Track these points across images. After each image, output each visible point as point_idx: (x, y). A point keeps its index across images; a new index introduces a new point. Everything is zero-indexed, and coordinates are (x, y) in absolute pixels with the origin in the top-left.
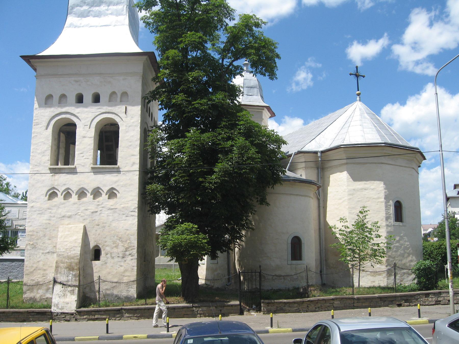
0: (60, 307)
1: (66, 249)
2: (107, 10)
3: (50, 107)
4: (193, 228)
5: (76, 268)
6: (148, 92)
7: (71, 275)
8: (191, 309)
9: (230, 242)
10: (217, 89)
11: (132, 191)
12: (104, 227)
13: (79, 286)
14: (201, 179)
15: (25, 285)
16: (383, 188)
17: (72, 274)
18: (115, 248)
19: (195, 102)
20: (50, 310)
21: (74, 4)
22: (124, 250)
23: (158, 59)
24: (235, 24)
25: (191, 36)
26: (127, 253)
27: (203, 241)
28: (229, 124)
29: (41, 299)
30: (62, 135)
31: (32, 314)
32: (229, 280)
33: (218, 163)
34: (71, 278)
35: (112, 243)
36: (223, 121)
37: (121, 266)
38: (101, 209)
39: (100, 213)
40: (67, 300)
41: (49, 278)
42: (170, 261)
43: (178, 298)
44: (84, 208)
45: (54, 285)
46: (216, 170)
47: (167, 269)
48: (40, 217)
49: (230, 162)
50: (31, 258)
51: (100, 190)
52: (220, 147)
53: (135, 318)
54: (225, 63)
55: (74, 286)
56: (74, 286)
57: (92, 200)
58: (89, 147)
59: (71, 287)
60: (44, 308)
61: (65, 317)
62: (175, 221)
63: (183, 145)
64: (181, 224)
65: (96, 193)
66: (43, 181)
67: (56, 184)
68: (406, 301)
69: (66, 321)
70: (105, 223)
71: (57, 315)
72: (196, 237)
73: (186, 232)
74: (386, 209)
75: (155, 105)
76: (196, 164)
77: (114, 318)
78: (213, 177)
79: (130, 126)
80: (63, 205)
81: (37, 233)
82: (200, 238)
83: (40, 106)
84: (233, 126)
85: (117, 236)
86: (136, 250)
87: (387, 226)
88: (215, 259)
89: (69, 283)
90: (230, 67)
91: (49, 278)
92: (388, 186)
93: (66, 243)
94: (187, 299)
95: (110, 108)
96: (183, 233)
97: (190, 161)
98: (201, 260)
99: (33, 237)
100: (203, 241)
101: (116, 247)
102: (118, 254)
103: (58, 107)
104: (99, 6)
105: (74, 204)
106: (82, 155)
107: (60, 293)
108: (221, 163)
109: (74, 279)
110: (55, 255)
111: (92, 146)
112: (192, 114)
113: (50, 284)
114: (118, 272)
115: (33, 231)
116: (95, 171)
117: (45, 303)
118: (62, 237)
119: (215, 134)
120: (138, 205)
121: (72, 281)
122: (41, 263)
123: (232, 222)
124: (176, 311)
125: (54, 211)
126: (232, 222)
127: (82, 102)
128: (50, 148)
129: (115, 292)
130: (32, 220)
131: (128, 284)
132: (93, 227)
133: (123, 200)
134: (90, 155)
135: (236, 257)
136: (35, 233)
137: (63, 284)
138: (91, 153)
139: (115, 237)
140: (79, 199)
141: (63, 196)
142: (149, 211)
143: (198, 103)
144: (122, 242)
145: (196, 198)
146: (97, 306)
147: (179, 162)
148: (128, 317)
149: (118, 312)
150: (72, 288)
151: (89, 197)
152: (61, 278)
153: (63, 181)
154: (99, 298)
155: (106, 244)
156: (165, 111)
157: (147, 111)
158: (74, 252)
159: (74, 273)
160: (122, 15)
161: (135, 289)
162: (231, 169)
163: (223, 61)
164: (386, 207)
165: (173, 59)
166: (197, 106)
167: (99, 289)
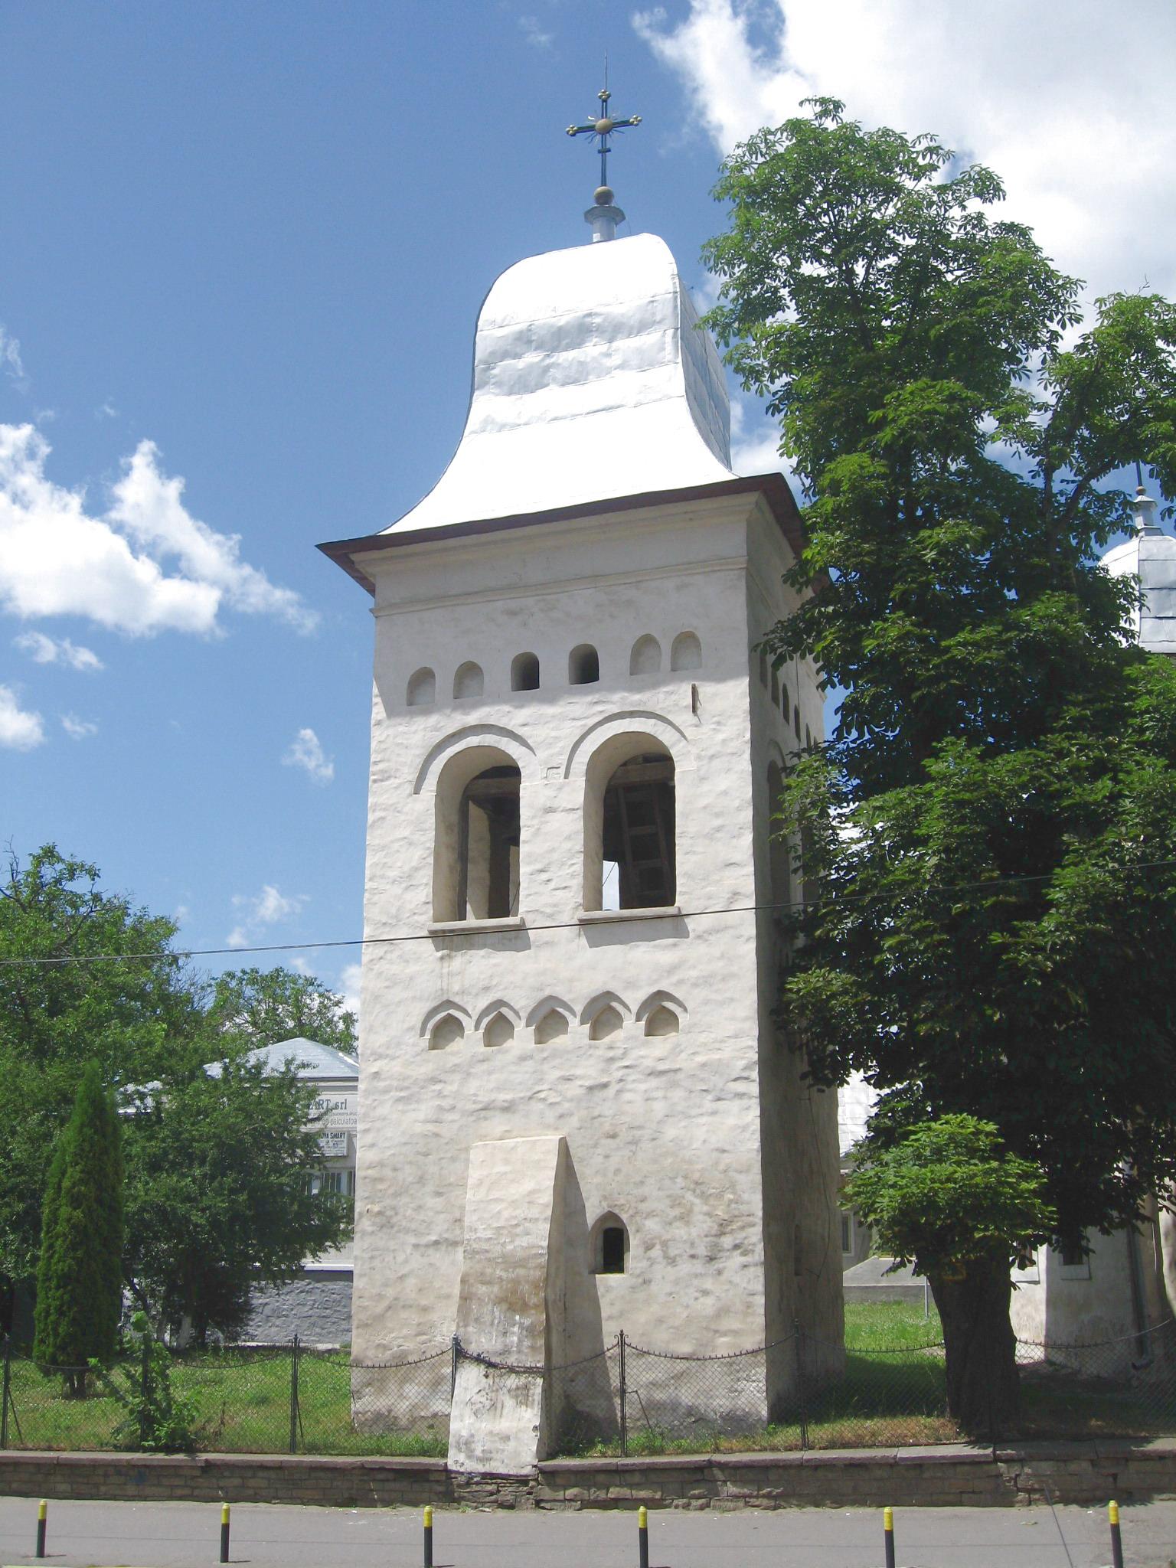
0: (478, 1453)
2: (608, 355)
3: (427, 712)
4: (977, 1133)
5: (534, 1300)
6: (770, 627)
7: (516, 1329)
8: (986, 1467)
9: (1137, 1186)
10: (1031, 588)
11: (732, 1000)
12: (635, 1142)
13: (547, 1373)
14: (996, 938)
15: (358, 1364)
17: (521, 1326)
18: (678, 1224)
19: (952, 642)
20: (442, 1461)
21: (492, 353)
22: (715, 1229)
23: (803, 503)
24: (1085, 337)
25: (914, 399)
26: (727, 1241)
27: (1024, 1185)
28: (1095, 714)
29: (413, 1421)
30: (474, 810)
31: (380, 1476)
32: (1141, 1344)
33: (1063, 868)
34: (515, 1339)
35: (668, 1202)
36: (1068, 703)
37: (706, 1293)
38: (619, 1074)
39: (619, 1092)
40: (504, 1425)
41: (439, 1338)
42: (894, 1268)
43: (933, 1421)
44: (557, 1074)
45: (455, 1369)
46: (1057, 895)
47: (889, 1307)
48: (404, 1112)
49: (1114, 859)
50: (376, 1263)
51: (614, 1004)
52: (1066, 803)
53: (765, 1502)
54: (1056, 487)
55: (530, 1371)
56: (530, 1371)
57: (587, 1041)
58: (568, 845)
59: (517, 1373)
60: (424, 1453)
61: (496, 1490)
62: (906, 1111)
63: (919, 810)
64: (929, 1120)
66: (411, 979)
67: (456, 988)
69: (502, 1506)
70: (640, 1128)
71: (468, 1484)
72: (994, 1170)
73: (955, 1149)
75: (802, 673)
76: (975, 877)
77: (681, 1502)
78: (1048, 923)
79: (712, 757)
80: (485, 1066)
81: (395, 1170)
82: (1008, 1175)
83: (391, 712)
84: (1112, 719)
85: (685, 1177)
86: (759, 1229)
88: (1080, 1262)
89: (512, 1360)
90: (1082, 504)
91: (439, 1338)
93: (498, 1207)
94: (973, 1428)
95: (637, 697)
96: (939, 1155)
97: (947, 869)
98: (1022, 1267)
99: (380, 1187)
100: (1024, 1185)
101: (681, 1218)
102: (692, 1244)
103: (455, 709)
104: (579, 345)
105: (523, 1058)
106: (544, 876)
107: (477, 1398)
108: (1076, 865)
109: (527, 1343)
110: (461, 1249)
111: (579, 843)
112: (943, 686)
113: (441, 1365)
114: (695, 1315)
115: (381, 1164)
116: (595, 928)
117: (428, 1437)
118: (480, 1183)
119: (1042, 754)
120: (759, 1053)
121: (519, 1352)
122: (411, 1282)
123: (1138, 1108)
124: (926, 1475)
125: (449, 1089)
126: (1138, 1108)
128: (431, 860)
129: (686, 1396)
130: (378, 1124)
131: (731, 1361)
132: (595, 1146)
133: (702, 1038)
134: (573, 876)
135: (1164, 1251)
136: (388, 1172)
137: (490, 1365)
138: (572, 871)
139: (679, 1180)
140: (539, 1042)
141: (481, 1031)
142: (804, 1076)
143: (965, 644)
144: (704, 1197)
145: (982, 1015)
146: (619, 1451)
147: (907, 877)
148: (736, 1497)
149: (699, 1476)
150: (522, 1380)
151: (577, 1030)
152: (482, 1342)
153: (484, 974)
154: (623, 1418)
155: (644, 1207)
156: (839, 695)
157: (775, 699)
158: (524, 1241)
159: (527, 1322)
160: (661, 364)
161: (762, 1385)
162: (1120, 887)
163: (1048, 479)
165: (853, 488)
166: (959, 653)
167: (623, 1382)
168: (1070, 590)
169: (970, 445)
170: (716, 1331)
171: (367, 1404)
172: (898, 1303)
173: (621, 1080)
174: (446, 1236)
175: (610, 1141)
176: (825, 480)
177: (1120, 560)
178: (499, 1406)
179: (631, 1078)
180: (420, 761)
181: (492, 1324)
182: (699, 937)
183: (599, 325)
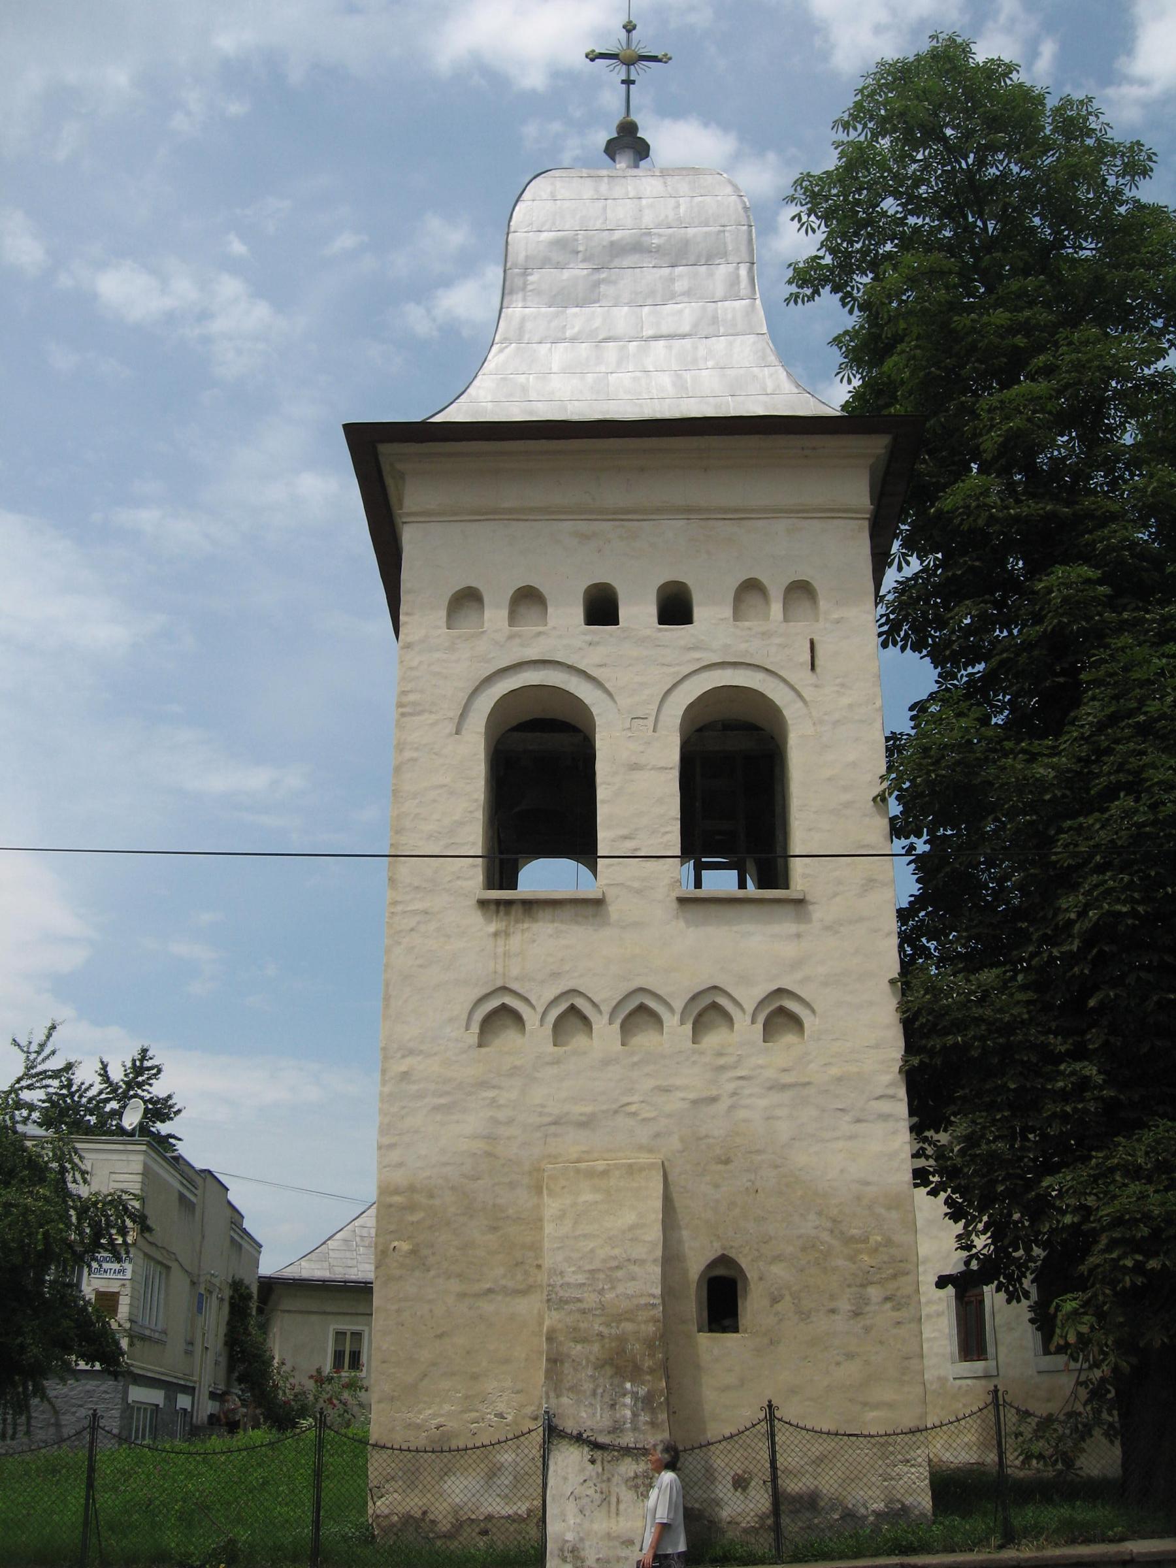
1: (592, 1272)
5: (648, 1363)
7: (628, 1400)
17: (635, 1395)
34: (628, 1413)
38: (731, 1087)
44: (651, 1083)
65: (708, 1011)
67: (515, 971)
79: (836, 723)
85: (820, 1214)
89: (628, 1439)
105: (606, 1062)
115: (412, 1189)
118: (562, 1216)
121: (635, 1429)
127: (615, 622)
137: (596, 1446)
139: (812, 1216)
151: (676, 1028)
153: (544, 957)
158: (631, 1288)
159: (642, 1391)
170: (865, 1404)
171: (390, 1504)
173: (734, 1094)
174: (503, 1282)
175: (720, 1167)
178: (614, 1500)
179: (746, 1092)
180: (463, 697)
181: (594, 1393)
182: (828, 928)
183: (659, 247)
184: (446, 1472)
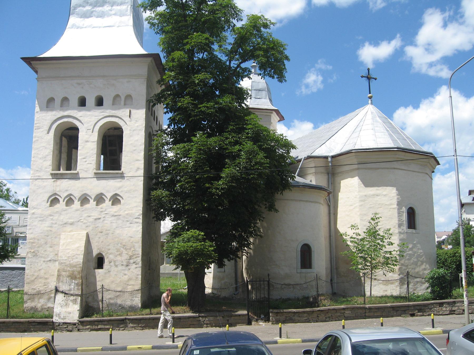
0: (62, 317)
1: (68, 257)
2: (111, 10)
3: (52, 110)
4: (199, 235)
5: (78, 276)
6: (152, 95)
7: (73, 284)
8: (197, 319)
9: (238, 249)
10: (224, 92)
11: (136, 197)
12: (108, 234)
13: (81, 296)
14: (207, 185)
15: (26, 294)
16: (395, 194)
17: (75, 283)
18: (118, 256)
19: (201, 106)
20: (52, 320)
21: (76, 5)
22: (129, 258)
23: (164, 61)
24: (243, 25)
26: (132, 261)
27: (210, 249)
28: (236, 128)
29: (42, 309)
30: (64, 139)
31: (33, 324)
32: (236, 289)
33: (225, 168)
34: (73, 287)
35: (116, 250)
36: (230, 125)
37: (125, 274)
38: (104, 215)
39: (104, 220)
40: (69, 309)
41: (50, 287)
42: (176, 269)
43: (184, 308)
44: (86, 215)
45: (55, 295)
46: (223, 175)
47: (173, 277)
48: (41, 224)
49: (238, 167)
50: (32, 266)
51: (103, 197)
52: (227, 151)
53: (140, 328)
54: (232, 65)
55: (77, 295)
56: (77, 295)
57: (95, 206)
58: (92, 152)
59: (73, 296)
60: (46, 317)
61: (68, 327)
62: (181, 229)
63: (189, 150)
65: (100, 199)
66: (45, 187)
67: (58, 190)
68: (420, 311)
69: (68, 331)
70: (109, 230)
71: (59, 325)
72: (203, 244)
73: (192, 239)
74: (398, 216)
75: (160, 109)
76: (203, 169)
77: (118, 329)
78: (220, 182)
79: (134, 130)
80: (66, 212)
81: (38, 240)
82: (206, 246)
83: (41, 109)
84: (241, 130)
85: (121, 244)
86: (140, 258)
87: (400, 233)
88: (222, 268)
89: (72, 292)
90: (238, 70)
91: (50, 287)
92: (400, 192)
93: (69, 251)
94: (193, 309)
95: (114, 112)
96: (189, 240)
97: (196, 166)
98: (208, 269)
99: (35, 245)
100: (210, 249)
101: (119, 255)
102: (122, 262)
103: (60, 110)
104: (103, 6)
105: (77, 210)
106: (85, 160)
107: (62, 303)
108: (229, 168)
109: (76, 288)
110: (57, 263)
111: (95, 151)
112: (198, 117)
113: (51, 294)
114: (122, 281)
115: (34, 238)
116: (98, 176)
117: (47, 313)
118: (64, 244)
119: (222, 138)
120: (143, 211)
121: (74, 290)
122: (42, 272)
123: (239, 229)
124: (182, 321)
125: (55, 218)
126: (239, 229)
127: (85, 106)
128: (52, 153)
129: (119, 302)
130: (33, 227)
131: (132, 293)
132: (96, 235)
133: (127, 207)
134: (93, 160)
135: (244, 265)
136: (36, 241)
137: (66, 294)
138: (94, 158)
139: (119, 245)
140: (81, 206)
141: (65, 202)
142: (154, 218)
143: (204, 107)
144: (126, 249)
145: (202, 204)
146: (101, 316)
147: (185, 167)
148: (132, 327)
149: (122, 322)
150: (75, 298)
151: (92, 203)
152: (63, 287)
153: (65, 187)
154: (102, 307)
155: (110, 251)
156: (170, 115)
157: (152, 115)
158: (76, 260)
159: (76, 282)
160: (126, 15)
161: (140, 298)
162: (239, 174)
163: (230, 63)
164: (399, 213)
165: (178, 61)
166: (203, 109)
167: (102, 298)
168: (233, 95)
169: (210, 51)
172: (171, 277)
176: (171, 57)
177: (245, 83)
184: (40, 298)
